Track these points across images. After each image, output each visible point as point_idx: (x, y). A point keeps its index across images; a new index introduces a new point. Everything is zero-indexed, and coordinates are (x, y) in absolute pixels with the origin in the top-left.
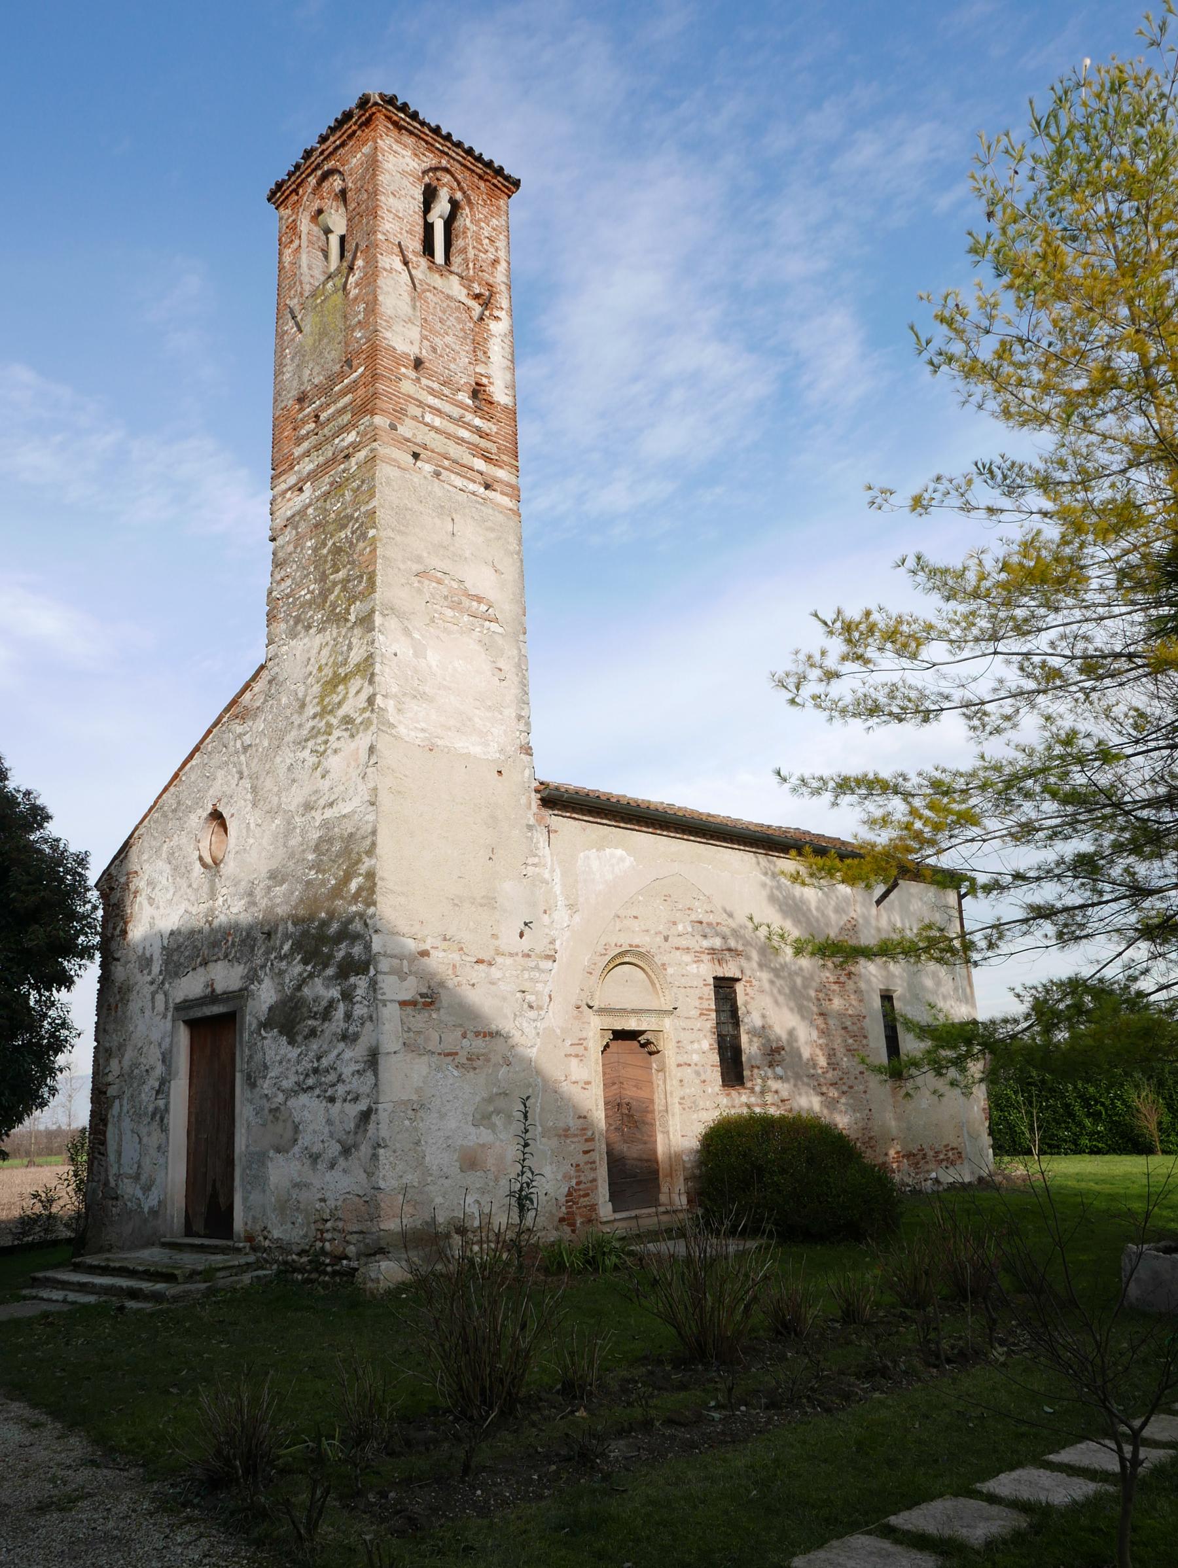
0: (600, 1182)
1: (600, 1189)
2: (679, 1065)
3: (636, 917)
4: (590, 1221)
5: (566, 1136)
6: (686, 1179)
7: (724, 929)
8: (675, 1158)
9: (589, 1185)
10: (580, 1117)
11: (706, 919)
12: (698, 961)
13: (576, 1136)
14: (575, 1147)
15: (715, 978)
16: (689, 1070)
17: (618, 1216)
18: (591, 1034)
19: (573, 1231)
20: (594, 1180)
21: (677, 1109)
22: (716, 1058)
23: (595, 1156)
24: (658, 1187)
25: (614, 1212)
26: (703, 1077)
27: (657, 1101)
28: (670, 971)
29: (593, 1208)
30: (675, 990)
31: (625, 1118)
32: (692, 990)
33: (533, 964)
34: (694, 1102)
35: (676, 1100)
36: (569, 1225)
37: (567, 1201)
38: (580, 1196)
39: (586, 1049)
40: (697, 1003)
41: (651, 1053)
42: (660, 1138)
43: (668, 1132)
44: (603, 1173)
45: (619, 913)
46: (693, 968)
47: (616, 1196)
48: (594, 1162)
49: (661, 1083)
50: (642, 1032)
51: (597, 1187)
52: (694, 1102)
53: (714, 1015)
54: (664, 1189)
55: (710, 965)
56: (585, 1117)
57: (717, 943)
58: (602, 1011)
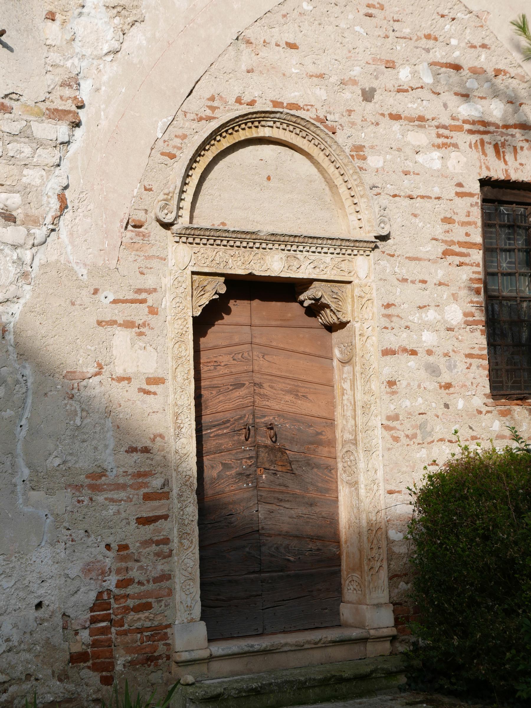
0: (178, 580)
1: (179, 596)
2: (387, 352)
3: (292, 46)
4: (151, 659)
5: (95, 488)
6: (393, 577)
7: (514, 83)
8: (375, 533)
9: (151, 586)
10: (132, 450)
11: (468, 61)
12: (445, 146)
13: (123, 487)
14: (118, 513)
15: (484, 183)
16: (412, 362)
17: (219, 648)
18: (167, 281)
19: (107, 681)
20: (166, 577)
21: (379, 437)
22: (478, 340)
23: (170, 528)
24: (338, 591)
25: (210, 640)
26: (446, 378)
27: (339, 422)
28: (374, 161)
29: (160, 632)
30: (384, 200)
31: (263, 454)
32: (428, 204)
33: (16, 127)
34: (422, 427)
35: (377, 421)
36: (95, 668)
37: (94, 620)
38: (127, 610)
39: (153, 311)
40: (439, 230)
41: (331, 328)
42: (344, 495)
43: (356, 483)
44: (187, 561)
45: (249, 34)
46: (433, 159)
47: (219, 609)
48: (166, 541)
49: (347, 386)
50: (305, 284)
51: (170, 592)
52: (422, 427)
53: (477, 256)
54: (350, 592)
55: (475, 155)
56: (146, 450)
57: (496, 111)
58: (193, 235)
